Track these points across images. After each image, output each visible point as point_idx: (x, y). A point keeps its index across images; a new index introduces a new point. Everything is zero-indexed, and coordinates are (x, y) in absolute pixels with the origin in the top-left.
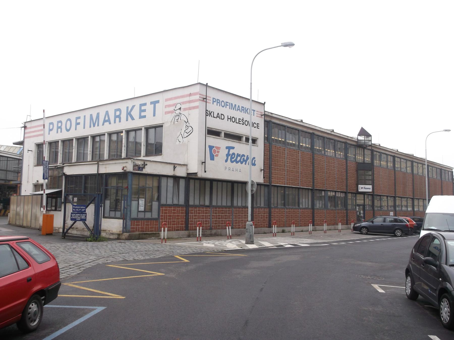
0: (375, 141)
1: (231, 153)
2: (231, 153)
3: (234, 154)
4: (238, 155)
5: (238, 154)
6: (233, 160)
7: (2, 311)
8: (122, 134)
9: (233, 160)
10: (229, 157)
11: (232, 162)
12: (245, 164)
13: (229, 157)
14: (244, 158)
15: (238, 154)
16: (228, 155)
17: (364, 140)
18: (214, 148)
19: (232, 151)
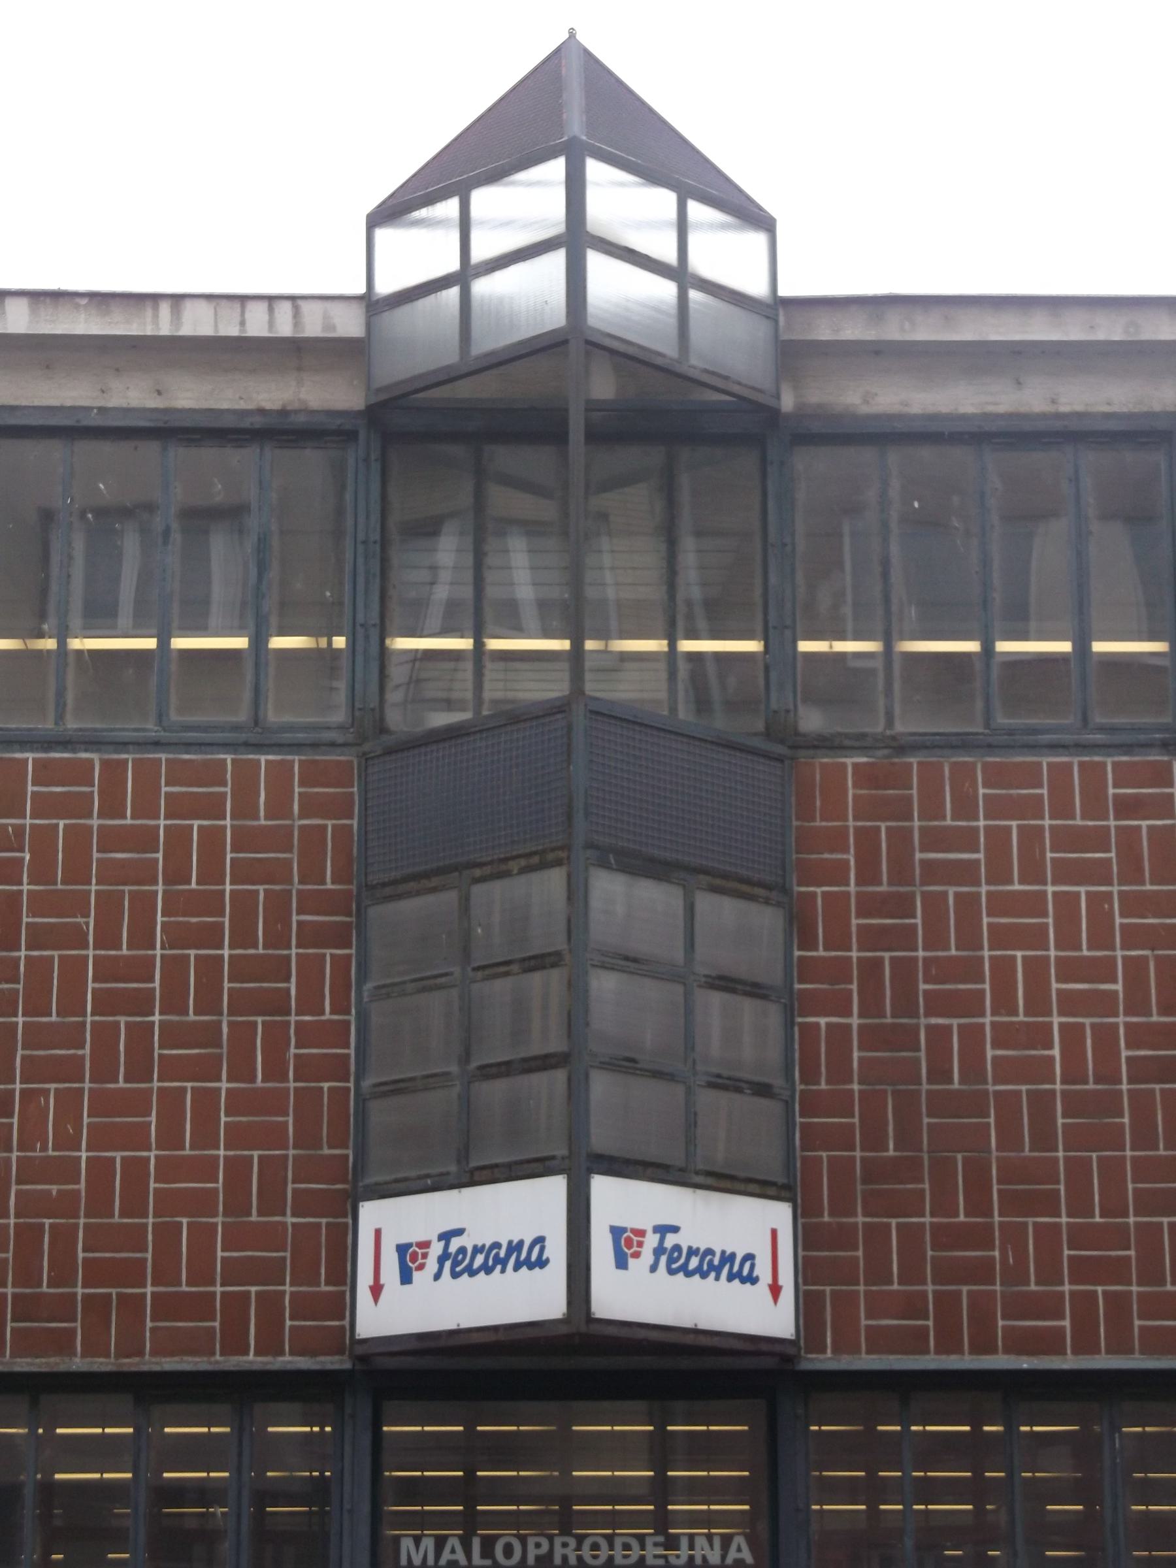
0: (845, 240)
1: (453, 1249)
2: (453, 1249)
3: (677, 1248)
4: (692, 1252)
5: (690, 1248)
6: (674, 1266)
7: (1174, 1215)
8: (54, 1193)
9: (674, 1266)
10: (448, 1264)
11: (671, 1272)
12: (717, 1278)
13: (448, 1264)
14: (711, 1261)
15: (690, 1248)
16: (659, 1251)
17: (466, 274)
18: (629, 1234)
19: (670, 1240)
